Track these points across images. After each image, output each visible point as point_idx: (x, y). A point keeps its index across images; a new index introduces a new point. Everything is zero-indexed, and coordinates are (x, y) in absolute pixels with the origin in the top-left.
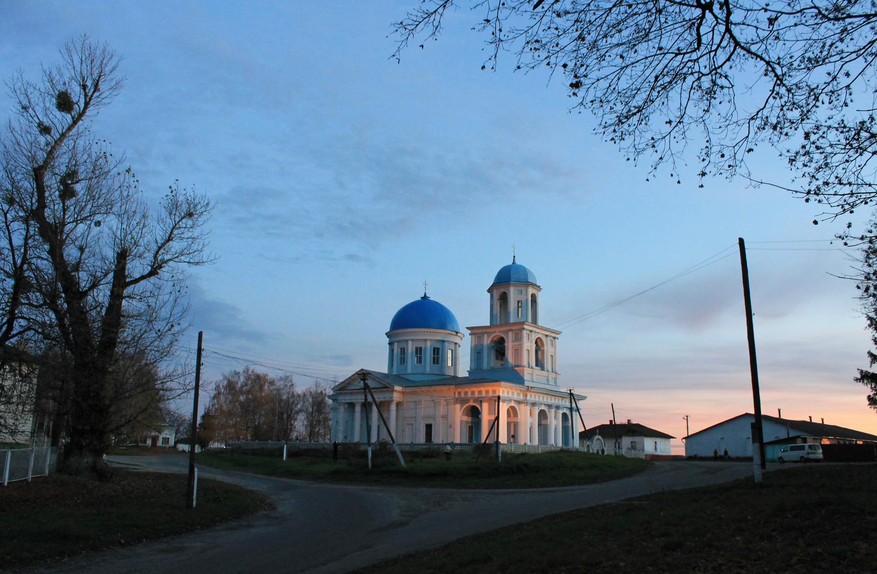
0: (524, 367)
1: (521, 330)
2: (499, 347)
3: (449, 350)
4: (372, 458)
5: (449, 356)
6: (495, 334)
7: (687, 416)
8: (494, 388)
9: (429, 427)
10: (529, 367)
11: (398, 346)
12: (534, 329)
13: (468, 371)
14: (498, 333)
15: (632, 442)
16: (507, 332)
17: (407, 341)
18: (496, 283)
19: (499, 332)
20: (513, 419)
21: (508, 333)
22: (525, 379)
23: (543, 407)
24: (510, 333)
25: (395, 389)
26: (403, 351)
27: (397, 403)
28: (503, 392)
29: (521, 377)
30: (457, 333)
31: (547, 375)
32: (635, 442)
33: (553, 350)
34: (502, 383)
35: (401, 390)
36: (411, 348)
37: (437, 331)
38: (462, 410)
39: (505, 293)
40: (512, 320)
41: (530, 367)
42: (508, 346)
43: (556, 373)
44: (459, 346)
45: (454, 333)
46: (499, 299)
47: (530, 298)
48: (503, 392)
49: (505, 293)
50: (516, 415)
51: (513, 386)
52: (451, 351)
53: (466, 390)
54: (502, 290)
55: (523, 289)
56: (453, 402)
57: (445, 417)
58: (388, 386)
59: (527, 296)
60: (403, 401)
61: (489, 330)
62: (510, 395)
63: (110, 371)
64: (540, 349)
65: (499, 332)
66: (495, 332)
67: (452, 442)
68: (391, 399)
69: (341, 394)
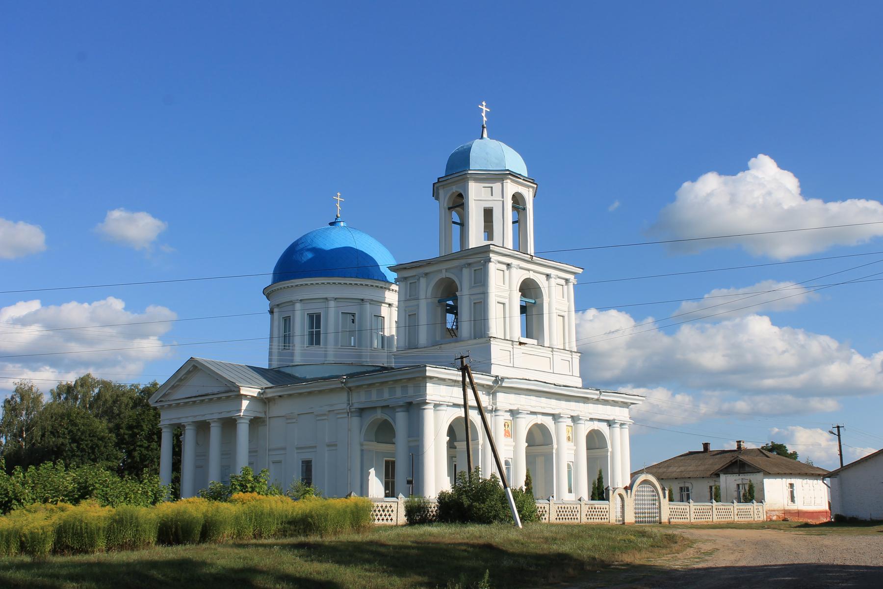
7: (838, 427)
17: (292, 303)
19: (446, 270)
21: (461, 270)
24: (466, 272)
47: (509, 203)
66: (441, 271)
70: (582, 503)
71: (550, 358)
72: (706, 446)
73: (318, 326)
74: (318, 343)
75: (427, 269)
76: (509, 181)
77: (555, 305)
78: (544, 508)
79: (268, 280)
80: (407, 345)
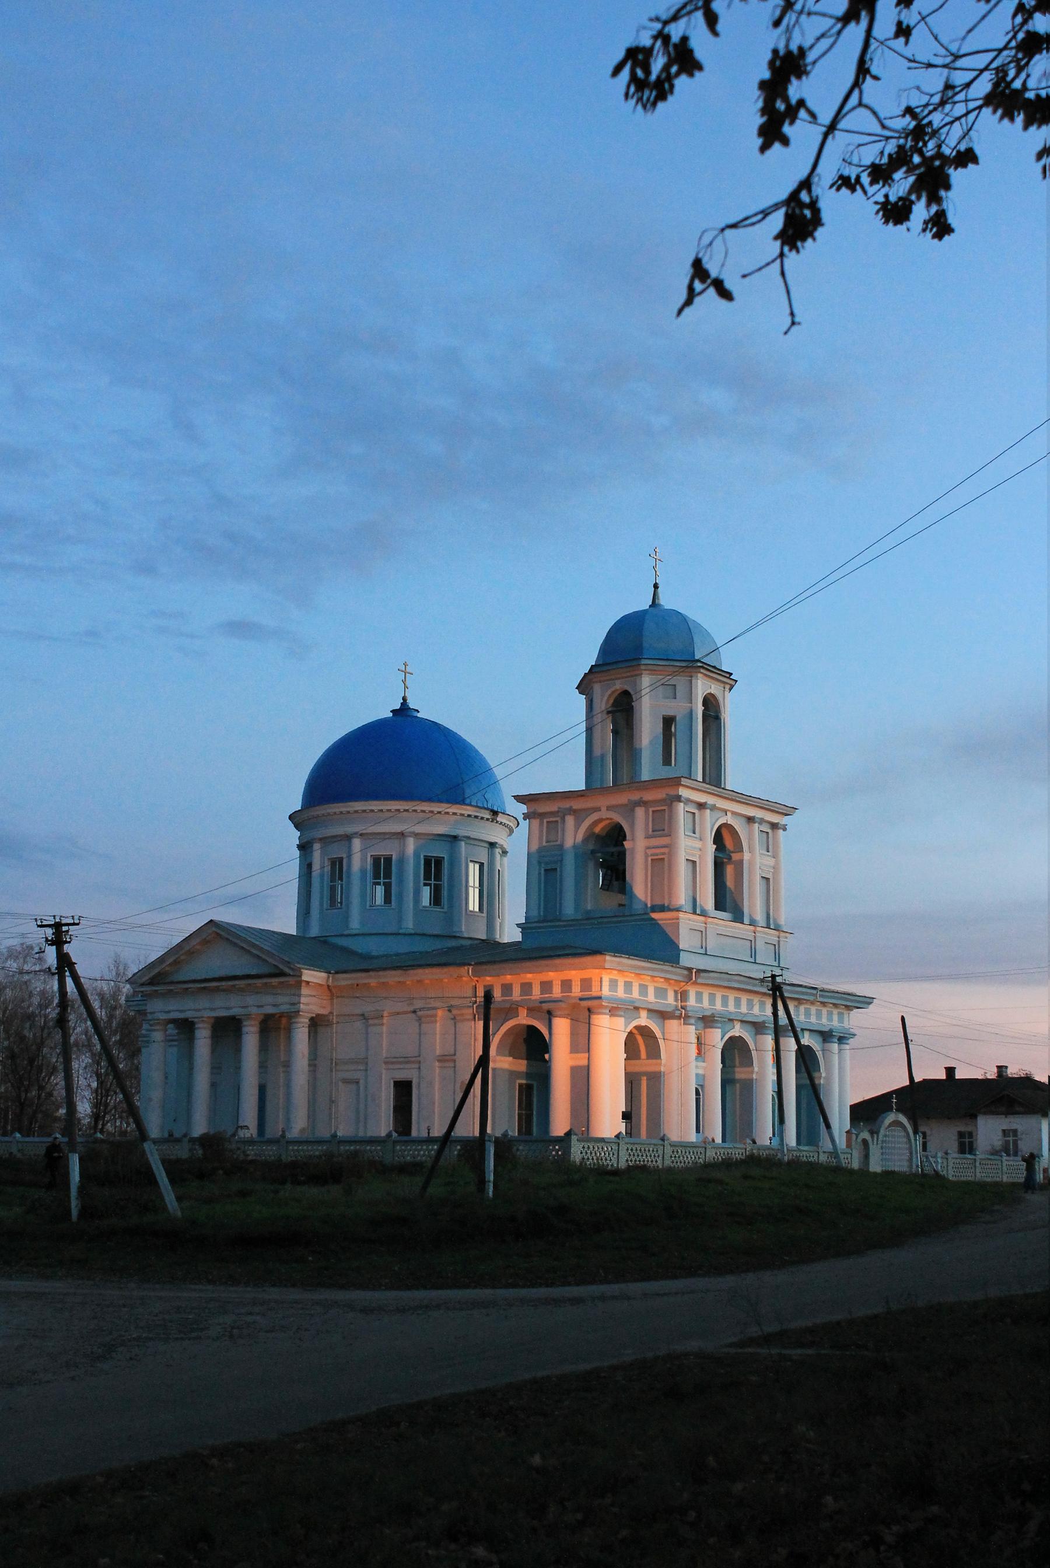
0: (678, 910)
1: (670, 806)
2: (612, 854)
3: (471, 865)
4: (81, 1189)
5: (471, 883)
6: (595, 817)
8: (591, 973)
9: (403, 1090)
10: (694, 913)
11: (323, 855)
12: (711, 800)
13: (518, 925)
15: (1005, 1132)
16: (630, 809)
17: (348, 838)
18: (605, 664)
19: (609, 808)
20: (644, 1065)
21: (633, 810)
23: (737, 1031)
24: (640, 812)
25: (304, 978)
26: (338, 868)
27: (312, 1019)
28: (613, 984)
30: (495, 813)
32: (1015, 1132)
33: (771, 862)
34: (608, 958)
35: (323, 983)
36: (359, 860)
37: (436, 807)
39: (626, 694)
40: (646, 775)
41: (698, 912)
42: (633, 850)
44: (505, 853)
45: (487, 815)
46: (608, 712)
47: (700, 709)
48: (613, 984)
49: (626, 694)
50: (654, 1052)
51: (644, 968)
52: (477, 866)
53: (509, 978)
54: (618, 686)
55: (680, 681)
56: (471, 1017)
58: (287, 970)
59: (690, 699)
60: (331, 1013)
61: (577, 805)
62: (636, 994)
64: (730, 858)
65: (609, 808)
66: (598, 809)
69: (155, 995)
70: (949, 1157)
71: (751, 941)
72: (950, 1071)
76: (700, 675)
77: (758, 860)
78: (657, 1151)
80: (542, 914)
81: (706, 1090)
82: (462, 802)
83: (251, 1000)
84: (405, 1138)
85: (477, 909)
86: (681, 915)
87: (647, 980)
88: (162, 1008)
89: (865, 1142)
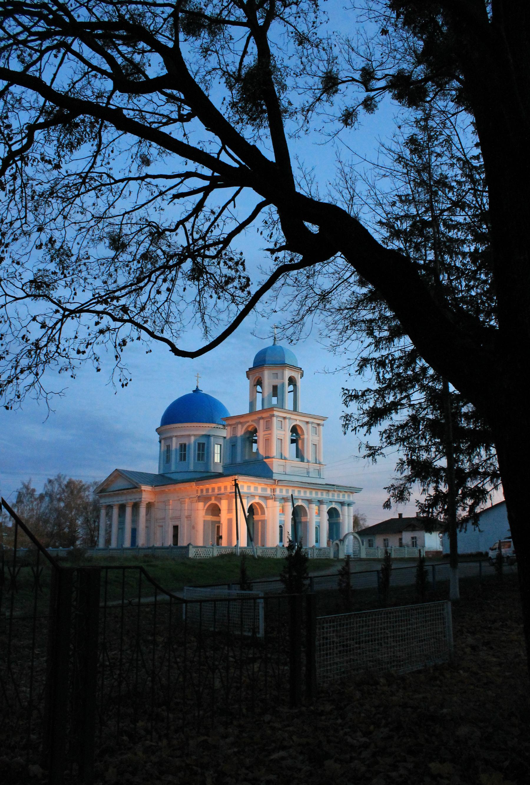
1: (271, 418)
3: (216, 446)
5: (216, 451)
6: (248, 424)
9: (176, 528)
10: (282, 459)
11: (165, 444)
14: (250, 423)
15: (413, 538)
19: (252, 421)
22: (274, 471)
24: (262, 422)
29: (270, 470)
31: (307, 467)
32: (416, 538)
38: (206, 508)
41: (283, 458)
43: (320, 464)
45: (221, 427)
52: (219, 446)
54: (257, 375)
55: (279, 372)
57: (189, 517)
59: (283, 378)
63: (472, 498)
66: (248, 422)
67: (153, 546)
68: (140, 500)
72: (400, 515)
73: (185, 450)
74: (185, 460)
75: (242, 420)
77: (311, 438)
79: (158, 425)
81: (285, 525)
82: (213, 422)
83: (129, 497)
84: (176, 546)
85: (219, 461)
86: (274, 459)
87: (257, 485)
88: (104, 501)
89: (337, 544)
